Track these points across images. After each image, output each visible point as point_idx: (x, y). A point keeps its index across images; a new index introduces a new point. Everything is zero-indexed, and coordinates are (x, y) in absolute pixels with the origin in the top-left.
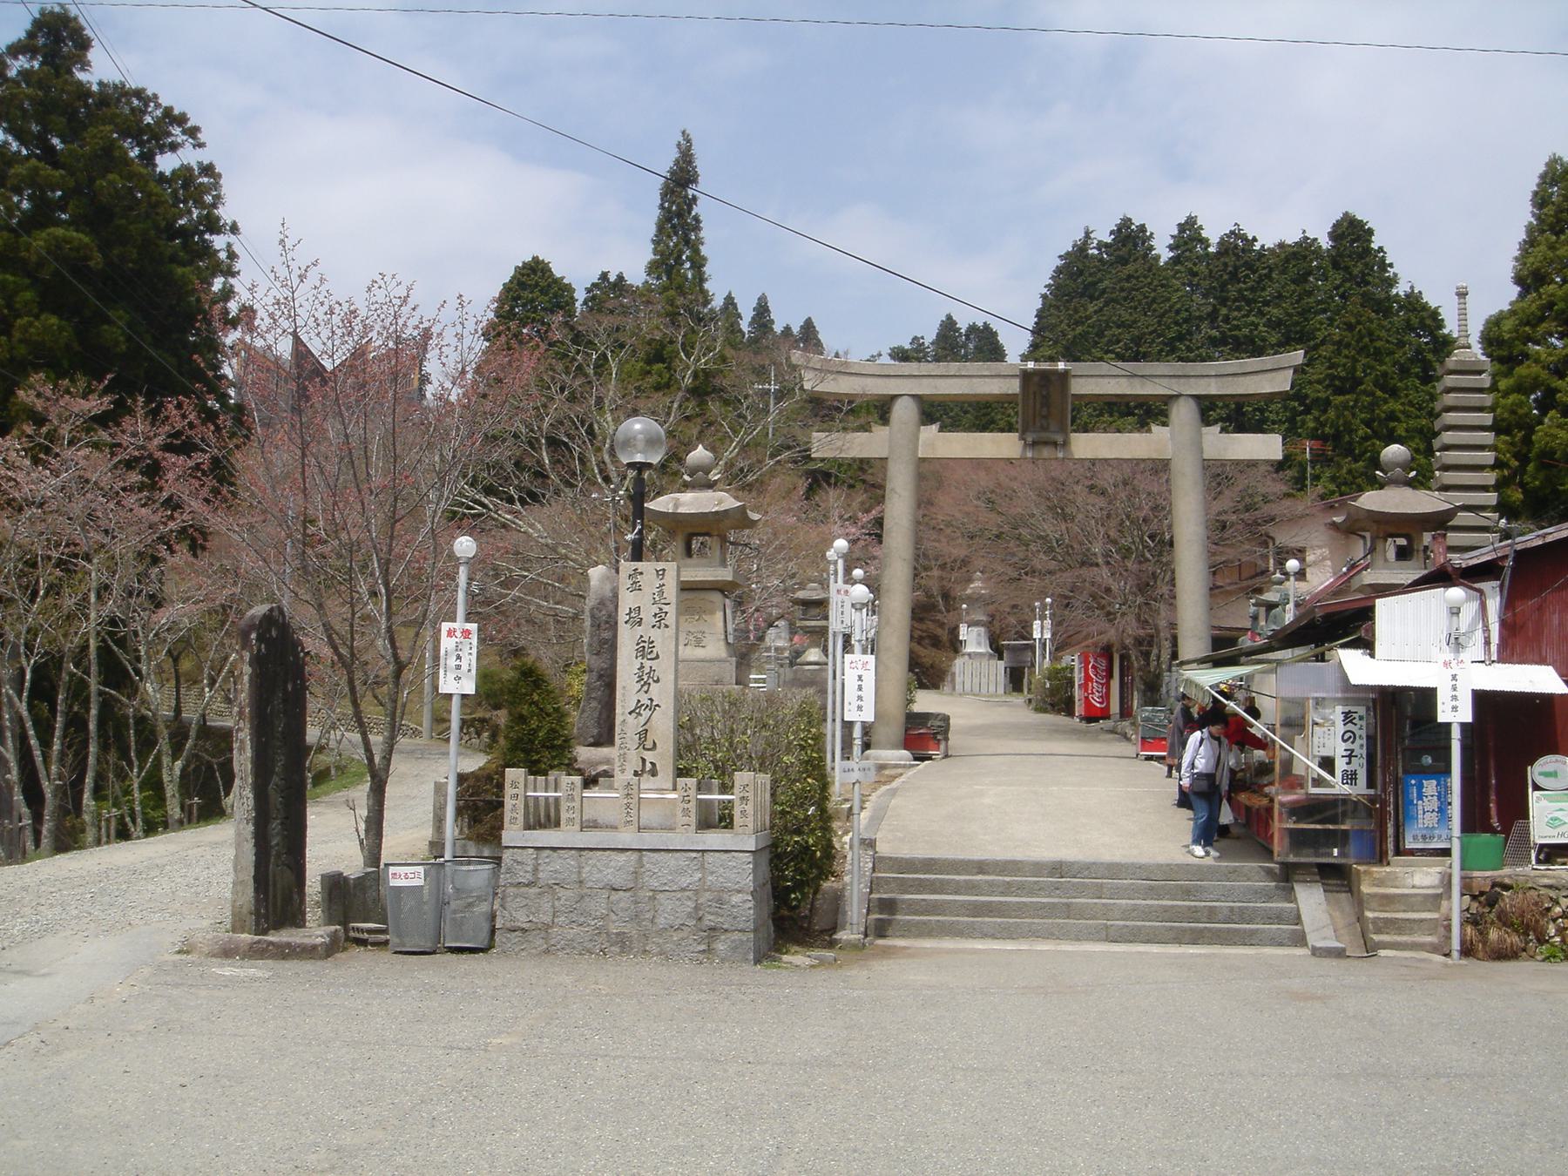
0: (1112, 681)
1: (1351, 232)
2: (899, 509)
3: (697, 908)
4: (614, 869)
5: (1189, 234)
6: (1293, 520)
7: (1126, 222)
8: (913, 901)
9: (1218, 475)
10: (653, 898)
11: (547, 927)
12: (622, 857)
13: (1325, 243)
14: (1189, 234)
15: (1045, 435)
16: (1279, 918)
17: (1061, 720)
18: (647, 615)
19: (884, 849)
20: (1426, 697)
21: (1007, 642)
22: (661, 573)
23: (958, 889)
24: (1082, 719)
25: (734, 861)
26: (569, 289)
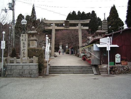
0: (73, 51)
1: (93, 12)
2: (53, 33)
3: (29, 72)
4: (20, 67)
5: (79, 12)
6: (89, 36)
7: (74, 11)
8: (55, 70)
9: (82, 30)
10: (24, 71)
11: (12, 74)
12: (21, 66)
13: (91, 13)
14: (79, 12)
15: (67, 27)
16: (91, 71)
17: (68, 54)
18: (24, 40)
19: (51, 65)
20: (105, 48)
21: (64, 47)
22: (25, 35)
23: (58, 69)
24: (70, 54)
25: (34, 66)
26: (24, 16)
